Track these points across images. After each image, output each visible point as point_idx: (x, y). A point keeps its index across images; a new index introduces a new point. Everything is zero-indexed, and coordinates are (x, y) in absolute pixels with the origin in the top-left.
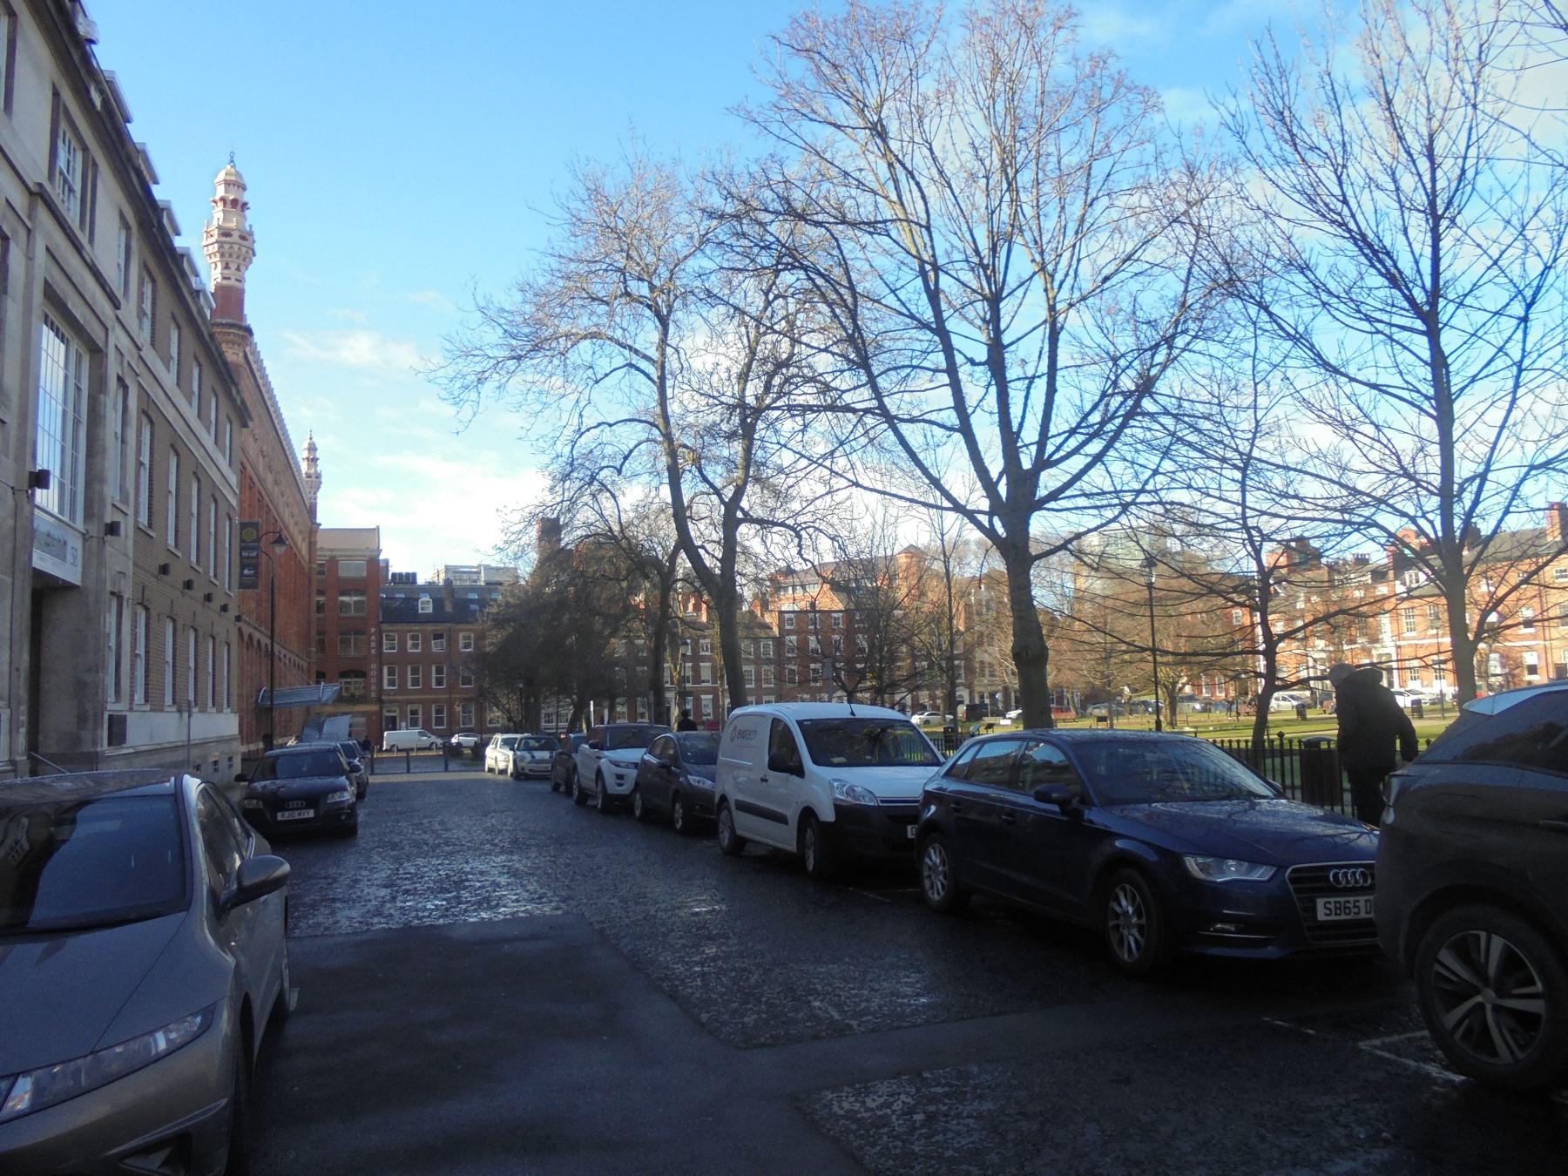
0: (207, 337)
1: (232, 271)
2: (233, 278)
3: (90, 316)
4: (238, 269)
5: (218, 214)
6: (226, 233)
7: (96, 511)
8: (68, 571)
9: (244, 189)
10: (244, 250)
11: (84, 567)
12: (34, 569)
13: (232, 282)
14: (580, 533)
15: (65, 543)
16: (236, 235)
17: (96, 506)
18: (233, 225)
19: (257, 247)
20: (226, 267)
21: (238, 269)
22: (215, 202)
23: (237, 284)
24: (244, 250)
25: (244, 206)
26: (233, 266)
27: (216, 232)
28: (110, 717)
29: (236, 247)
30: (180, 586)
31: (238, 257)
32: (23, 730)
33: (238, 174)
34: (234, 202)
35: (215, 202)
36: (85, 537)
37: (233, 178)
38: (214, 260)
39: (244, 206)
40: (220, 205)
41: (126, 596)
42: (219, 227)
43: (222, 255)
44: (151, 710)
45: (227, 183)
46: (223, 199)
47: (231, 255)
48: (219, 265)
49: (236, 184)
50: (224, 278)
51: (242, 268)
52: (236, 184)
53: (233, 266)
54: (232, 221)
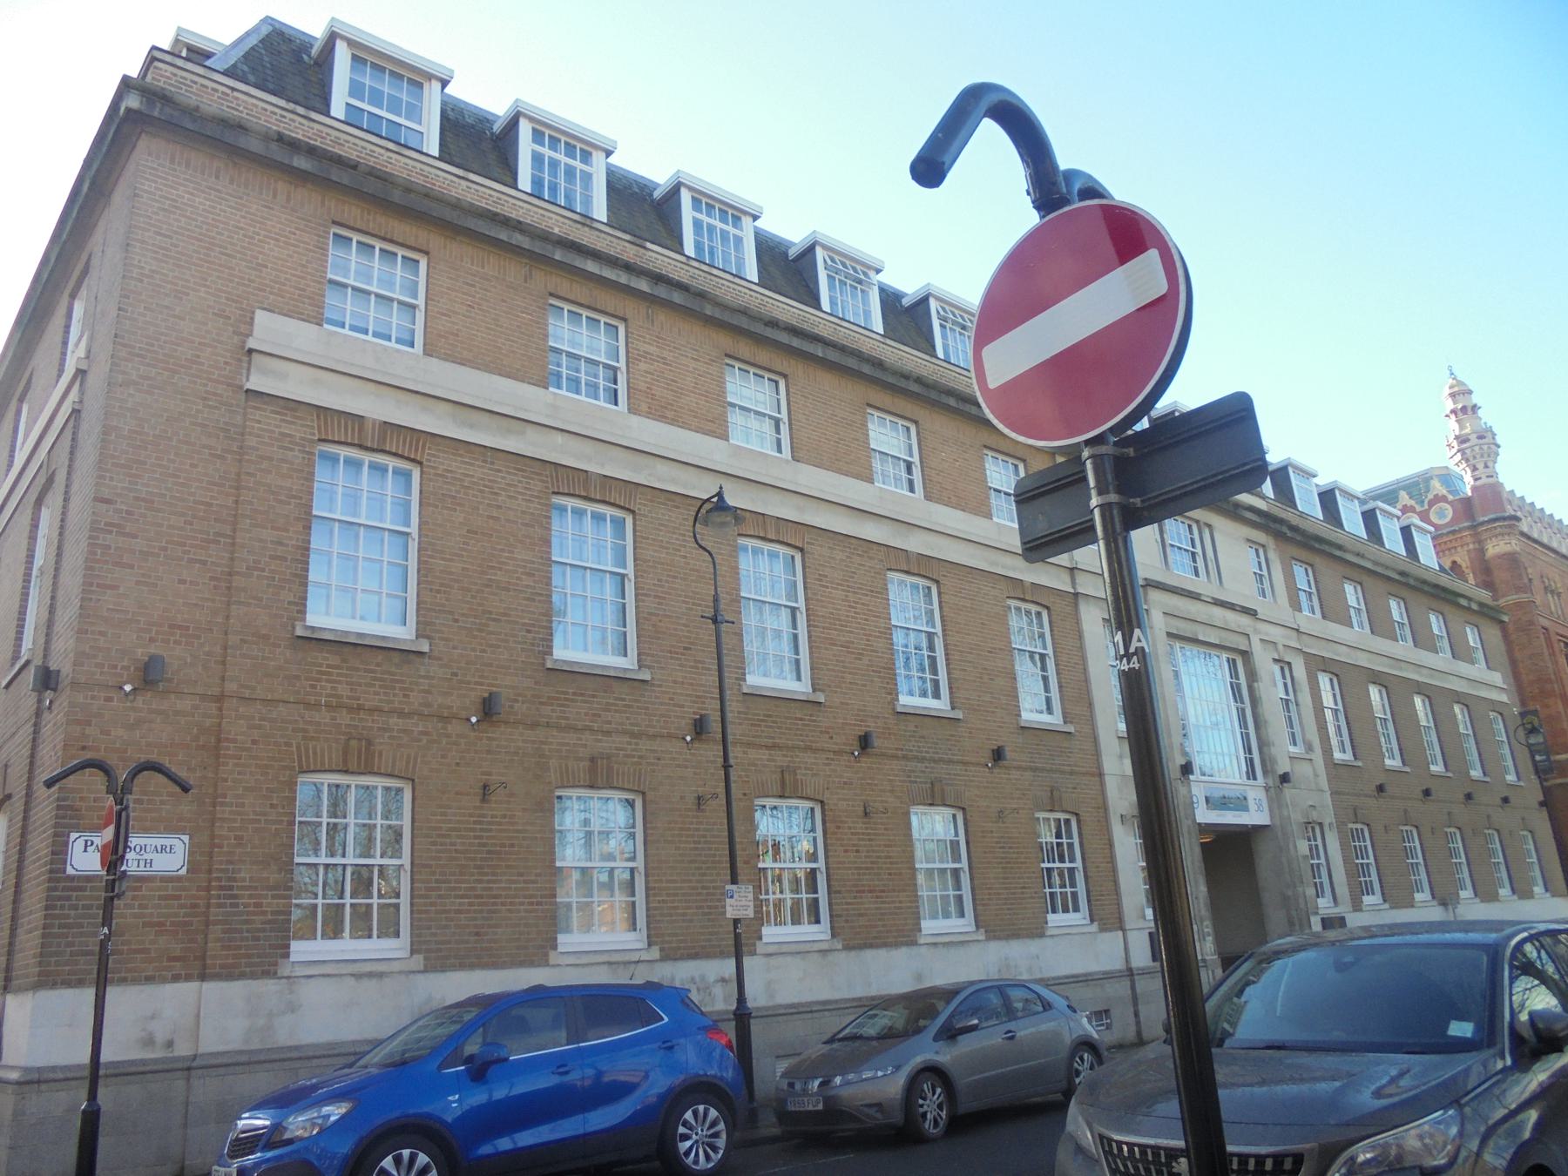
0: (1397, 577)
1: (1481, 470)
2: (1483, 476)
3: (1224, 634)
4: (1486, 466)
5: (1452, 426)
6: (1461, 439)
7: (1269, 768)
8: (1255, 816)
9: (1470, 392)
10: (1485, 447)
11: (1271, 810)
12: (1199, 824)
13: (1484, 481)
14: (889, 1013)
15: (1245, 798)
16: (1473, 437)
17: (1268, 764)
18: (1468, 431)
19: (1499, 440)
20: (1474, 469)
21: (1486, 466)
22: (1447, 416)
23: (1490, 480)
24: (1485, 447)
25: (1475, 408)
26: (1480, 466)
27: (1455, 444)
28: (1323, 920)
29: (1477, 448)
30: (1421, 796)
31: (1482, 456)
32: (1210, 939)
33: (1460, 383)
34: (1464, 409)
35: (1447, 416)
36: (1267, 789)
37: (1456, 389)
38: (1462, 467)
39: (1475, 408)
40: (1453, 416)
41: (1326, 823)
42: (1457, 438)
43: (1467, 460)
44: (1391, 908)
45: (1453, 395)
46: (1454, 411)
47: (1475, 458)
48: (1467, 469)
49: (1460, 392)
50: (1476, 480)
51: (1490, 464)
52: (1460, 392)
53: (1480, 466)
54: (1466, 428)
